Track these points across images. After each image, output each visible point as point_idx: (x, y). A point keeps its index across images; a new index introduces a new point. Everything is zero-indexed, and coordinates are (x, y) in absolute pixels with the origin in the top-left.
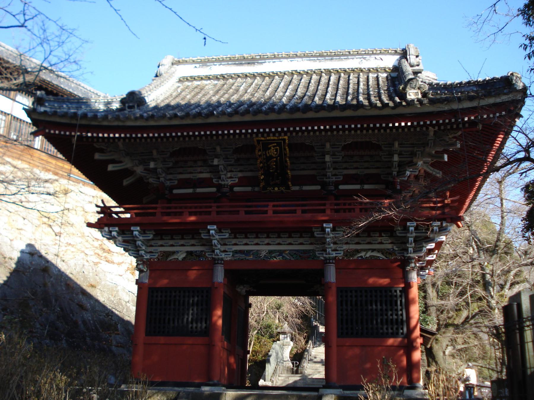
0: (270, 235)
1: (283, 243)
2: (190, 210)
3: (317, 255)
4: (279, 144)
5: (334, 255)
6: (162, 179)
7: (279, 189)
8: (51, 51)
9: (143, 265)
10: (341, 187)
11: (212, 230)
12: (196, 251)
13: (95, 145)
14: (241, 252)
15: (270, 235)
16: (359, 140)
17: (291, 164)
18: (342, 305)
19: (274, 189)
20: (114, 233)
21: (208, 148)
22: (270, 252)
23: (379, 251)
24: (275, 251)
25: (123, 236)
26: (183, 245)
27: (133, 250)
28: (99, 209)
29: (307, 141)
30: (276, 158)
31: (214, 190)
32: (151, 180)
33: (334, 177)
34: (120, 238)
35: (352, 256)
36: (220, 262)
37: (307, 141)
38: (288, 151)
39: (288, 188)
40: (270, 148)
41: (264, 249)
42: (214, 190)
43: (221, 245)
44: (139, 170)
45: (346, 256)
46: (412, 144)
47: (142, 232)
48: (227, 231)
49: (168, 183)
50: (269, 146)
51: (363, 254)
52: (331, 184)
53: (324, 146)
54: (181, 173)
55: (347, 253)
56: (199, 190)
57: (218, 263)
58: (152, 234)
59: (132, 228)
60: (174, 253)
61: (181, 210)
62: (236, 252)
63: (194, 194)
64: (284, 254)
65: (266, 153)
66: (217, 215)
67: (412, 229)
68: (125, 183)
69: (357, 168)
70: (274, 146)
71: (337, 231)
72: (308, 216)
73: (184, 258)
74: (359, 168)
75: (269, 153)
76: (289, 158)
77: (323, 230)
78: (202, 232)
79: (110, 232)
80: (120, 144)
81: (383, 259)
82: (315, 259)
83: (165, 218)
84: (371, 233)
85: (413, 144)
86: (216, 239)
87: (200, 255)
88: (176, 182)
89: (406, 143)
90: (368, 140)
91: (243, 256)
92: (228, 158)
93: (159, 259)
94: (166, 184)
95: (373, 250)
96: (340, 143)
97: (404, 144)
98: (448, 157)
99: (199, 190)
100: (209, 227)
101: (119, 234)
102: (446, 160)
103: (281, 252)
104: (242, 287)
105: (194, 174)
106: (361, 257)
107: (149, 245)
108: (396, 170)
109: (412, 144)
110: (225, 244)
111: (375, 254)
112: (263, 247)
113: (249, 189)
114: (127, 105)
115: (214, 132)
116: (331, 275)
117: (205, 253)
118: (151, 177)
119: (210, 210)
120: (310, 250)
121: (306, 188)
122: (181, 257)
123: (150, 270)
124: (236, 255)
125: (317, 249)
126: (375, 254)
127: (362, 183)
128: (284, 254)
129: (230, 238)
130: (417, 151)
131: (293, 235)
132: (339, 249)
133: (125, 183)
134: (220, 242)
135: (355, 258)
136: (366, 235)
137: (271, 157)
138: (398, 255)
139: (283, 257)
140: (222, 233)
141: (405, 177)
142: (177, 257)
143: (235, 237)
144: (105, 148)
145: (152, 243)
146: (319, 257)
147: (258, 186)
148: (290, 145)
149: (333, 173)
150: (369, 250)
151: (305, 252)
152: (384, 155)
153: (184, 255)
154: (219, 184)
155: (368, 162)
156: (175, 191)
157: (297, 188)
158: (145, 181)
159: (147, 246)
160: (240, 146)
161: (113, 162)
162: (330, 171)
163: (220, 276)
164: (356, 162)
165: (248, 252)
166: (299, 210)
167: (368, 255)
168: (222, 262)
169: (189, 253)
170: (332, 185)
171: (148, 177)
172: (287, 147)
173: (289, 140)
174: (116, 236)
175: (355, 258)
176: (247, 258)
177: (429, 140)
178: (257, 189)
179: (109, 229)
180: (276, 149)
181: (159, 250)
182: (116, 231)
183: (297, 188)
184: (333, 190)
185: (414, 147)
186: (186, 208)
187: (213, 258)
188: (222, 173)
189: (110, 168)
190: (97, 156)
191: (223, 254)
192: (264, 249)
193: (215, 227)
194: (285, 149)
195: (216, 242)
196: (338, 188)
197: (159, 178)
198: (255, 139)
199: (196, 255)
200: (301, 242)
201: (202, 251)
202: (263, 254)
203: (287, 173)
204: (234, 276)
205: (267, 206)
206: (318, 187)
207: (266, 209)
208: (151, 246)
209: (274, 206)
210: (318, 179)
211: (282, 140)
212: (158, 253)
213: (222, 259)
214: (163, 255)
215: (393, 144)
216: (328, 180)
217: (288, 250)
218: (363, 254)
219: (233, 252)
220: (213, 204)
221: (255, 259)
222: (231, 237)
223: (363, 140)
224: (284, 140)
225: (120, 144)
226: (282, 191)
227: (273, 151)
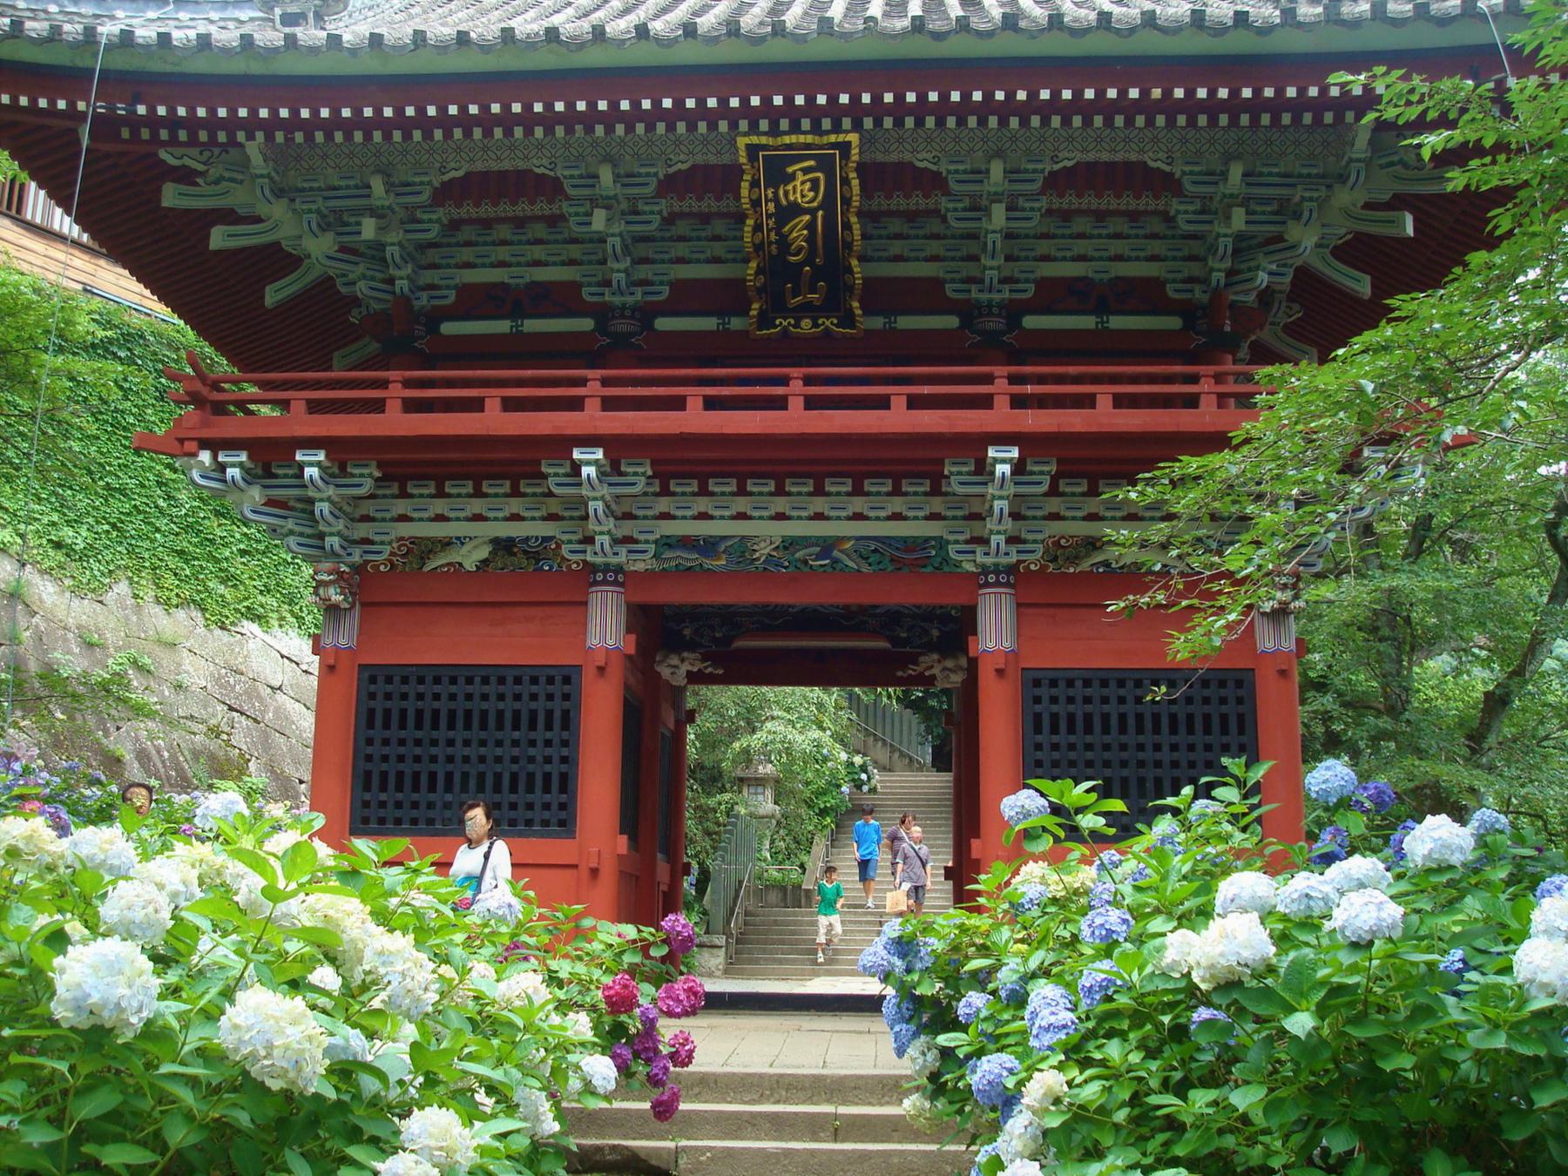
0: (868, 486)
1: (833, 513)
3: (953, 555)
4: (825, 164)
5: (1013, 558)
6: (402, 285)
7: (815, 325)
10: (1030, 322)
11: (588, 463)
12: (527, 539)
13: (163, 155)
14: (686, 542)
15: (868, 486)
16: (1105, 157)
17: (864, 236)
18: (1241, 718)
19: (797, 326)
20: (233, 473)
21: (567, 173)
22: (789, 544)
24: (805, 541)
26: (478, 518)
27: (301, 535)
28: (178, 388)
29: (919, 156)
30: (813, 212)
31: (586, 324)
32: (362, 288)
33: (639, 291)
35: (1074, 559)
37: (919, 156)
38: (856, 189)
39: (848, 319)
40: (793, 177)
42: (586, 324)
43: (616, 518)
44: (319, 247)
45: (1054, 559)
46: (973, 172)
49: (423, 300)
50: (790, 170)
52: (995, 310)
53: (981, 173)
54: (468, 265)
55: (1057, 551)
56: (532, 325)
57: (605, 582)
58: (370, 475)
59: (577, 454)
60: (446, 544)
62: (667, 543)
63: (517, 336)
64: (836, 553)
65: (776, 194)
67: (1003, 469)
68: (273, 295)
69: (1082, 258)
70: (806, 171)
71: (353, 476)
73: (485, 562)
74: (1092, 259)
75: (786, 193)
76: (859, 214)
77: (983, 468)
78: (551, 471)
79: (222, 468)
80: (254, 149)
82: (946, 569)
84: (485, 483)
85: (1212, 174)
86: (329, 499)
87: (538, 551)
88: (452, 296)
89: (1265, 170)
90: (1133, 157)
91: (690, 558)
92: (636, 213)
94: (415, 303)
96: (1040, 167)
97: (1261, 174)
98: (1415, 220)
99: (532, 325)
100: (577, 454)
101: (250, 476)
102: (1410, 231)
103: (827, 546)
104: (675, 660)
105: (659, 267)
106: (1106, 564)
107: (357, 516)
109: (973, 172)
110: (629, 516)
112: (764, 525)
113: (708, 323)
114: (278, 11)
115: (162, 111)
116: (996, 629)
117: (559, 546)
118: (364, 277)
120: (927, 539)
121: (906, 322)
122: (471, 557)
123: (363, 605)
124: (668, 554)
125: (565, 537)
127: (1102, 307)
128: (836, 553)
129: (645, 494)
130: (1303, 199)
131: (867, 487)
132: (1030, 537)
133: (273, 295)
134: (614, 506)
135: (1085, 566)
136: (433, 491)
137: (795, 210)
139: (836, 561)
141: (1247, 292)
142: (459, 559)
143: (665, 492)
144: (201, 168)
145: (368, 508)
146: (958, 564)
147: (744, 312)
148: (861, 169)
149: (1006, 273)
151: (909, 544)
152: (1186, 212)
153: (484, 553)
154: (604, 305)
155: (1081, 236)
156: (448, 328)
157: (877, 323)
158: (343, 290)
159: (352, 520)
160: (684, 167)
161: (229, 216)
162: (994, 263)
163: (605, 627)
164: (1081, 236)
165: (708, 546)
166: (1104, 395)
168: (621, 578)
169: (503, 546)
170: (999, 315)
171: (351, 276)
172: (853, 175)
174: (242, 484)
175: (1085, 566)
176: (709, 563)
177: (1351, 160)
178: (736, 323)
179: (215, 457)
180: (815, 182)
183: (877, 323)
184: (1003, 333)
185: (1294, 185)
187: (585, 562)
188: (616, 266)
189: (219, 238)
190: (172, 196)
191: (623, 550)
193: (599, 454)
194: (846, 181)
196: (651, 328)
197: (391, 281)
198: (742, 142)
199: (525, 552)
200: (477, 511)
201: (546, 539)
202: (764, 550)
203: (850, 270)
204: (656, 628)
205: (383, 384)
206: (952, 322)
207: (780, 390)
208: (366, 518)
209: (606, 382)
210: (949, 294)
211: (833, 146)
212: (390, 543)
213: (619, 569)
214: (409, 551)
215: (988, 171)
216: (984, 296)
217: (849, 539)
219: (656, 542)
220: (589, 373)
221: (734, 567)
222: (651, 490)
223: (1119, 157)
224: (845, 147)
225: (254, 149)
226: (827, 331)
227: (800, 190)
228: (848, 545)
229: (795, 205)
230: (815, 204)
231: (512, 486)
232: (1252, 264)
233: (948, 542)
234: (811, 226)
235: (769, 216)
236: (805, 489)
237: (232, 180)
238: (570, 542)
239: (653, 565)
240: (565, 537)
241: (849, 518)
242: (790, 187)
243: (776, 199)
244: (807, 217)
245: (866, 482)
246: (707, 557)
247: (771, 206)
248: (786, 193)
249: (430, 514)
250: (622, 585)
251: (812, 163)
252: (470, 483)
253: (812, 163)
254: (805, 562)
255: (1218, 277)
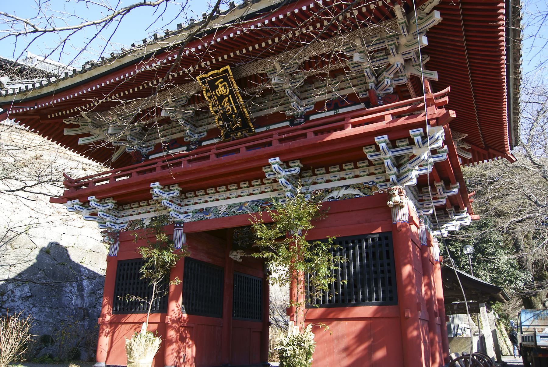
2: (188, 158)
8: (17, 36)
9: (112, 236)
14: (201, 211)
22: (230, 207)
23: (354, 187)
25: (287, 170)
30: (228, 96)
34: (85, 211)
36: (178, 225)
40: (218, 86)
41: (223, 204)
47: (285, 166)
48: (296, 164)
51: (335, 194)
59: (270, 161)
61: (178, 160)
62: (196, 212)
64: (243, 208)
65: (215, 93)
66: (247, 151)
70: (221, 83)
72: (142, 177)
75: (218, 92)
78: (266, 170)
81: (361, 197)
83: (224, 159)
91: (201, 216)
93: (127, 230)
95: (347, 187)
103: (241, 205)
104: (235, 253)
106: (333, 198)
108: (372, 80)
111: (350, 191)
115: (281, 17)
119: (155, 166)
126: (350, 191)
128: (243, 208)
138: (380, 188)
139: (244, 210)
140: (291, 167)
150: (342, 187)
167: (341, 195)
168: (182, 225)
173: (231, 69)
176: (207, 217)
181: (127, 220)
182: (157, 187)
186: (387, 109)
192: (223, 204)
195: (283, 180)
200: (327, 179)
202: (223, 209)
213: (182, 222)
217: (248, 202)
218: (335, 194)
219: (193, 212)
228: (247, 204)
229: (222, 95)
230: (227, 93)
231: (340, 168)
232: (383, 77)
233: (279, 198)
234: (229, 101)
235: (216, 101)
236: (336, 169)
237: (84, 125)
238: (380, 182)
239: (192, 220)
240: (377, 181)
241: (248, 195)
242: (218, 90)
243: (216, 95)
244: (227, 98)
245: (358, 163)
246: (206, 215)
247: (215, 97)
248: (218, 92)
249: (339, 177)
250: (182, 227)
251: (222, 80)
252: (247, 182)
253: (222, 80)
254: (234, 212)
255: (371, 85)
